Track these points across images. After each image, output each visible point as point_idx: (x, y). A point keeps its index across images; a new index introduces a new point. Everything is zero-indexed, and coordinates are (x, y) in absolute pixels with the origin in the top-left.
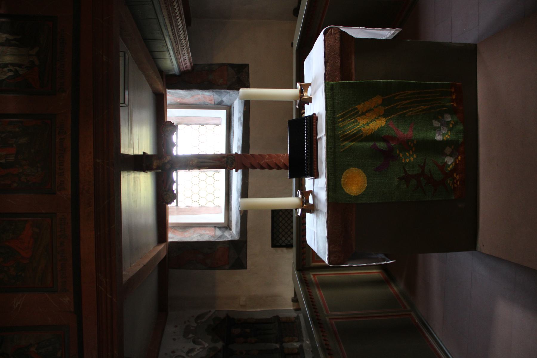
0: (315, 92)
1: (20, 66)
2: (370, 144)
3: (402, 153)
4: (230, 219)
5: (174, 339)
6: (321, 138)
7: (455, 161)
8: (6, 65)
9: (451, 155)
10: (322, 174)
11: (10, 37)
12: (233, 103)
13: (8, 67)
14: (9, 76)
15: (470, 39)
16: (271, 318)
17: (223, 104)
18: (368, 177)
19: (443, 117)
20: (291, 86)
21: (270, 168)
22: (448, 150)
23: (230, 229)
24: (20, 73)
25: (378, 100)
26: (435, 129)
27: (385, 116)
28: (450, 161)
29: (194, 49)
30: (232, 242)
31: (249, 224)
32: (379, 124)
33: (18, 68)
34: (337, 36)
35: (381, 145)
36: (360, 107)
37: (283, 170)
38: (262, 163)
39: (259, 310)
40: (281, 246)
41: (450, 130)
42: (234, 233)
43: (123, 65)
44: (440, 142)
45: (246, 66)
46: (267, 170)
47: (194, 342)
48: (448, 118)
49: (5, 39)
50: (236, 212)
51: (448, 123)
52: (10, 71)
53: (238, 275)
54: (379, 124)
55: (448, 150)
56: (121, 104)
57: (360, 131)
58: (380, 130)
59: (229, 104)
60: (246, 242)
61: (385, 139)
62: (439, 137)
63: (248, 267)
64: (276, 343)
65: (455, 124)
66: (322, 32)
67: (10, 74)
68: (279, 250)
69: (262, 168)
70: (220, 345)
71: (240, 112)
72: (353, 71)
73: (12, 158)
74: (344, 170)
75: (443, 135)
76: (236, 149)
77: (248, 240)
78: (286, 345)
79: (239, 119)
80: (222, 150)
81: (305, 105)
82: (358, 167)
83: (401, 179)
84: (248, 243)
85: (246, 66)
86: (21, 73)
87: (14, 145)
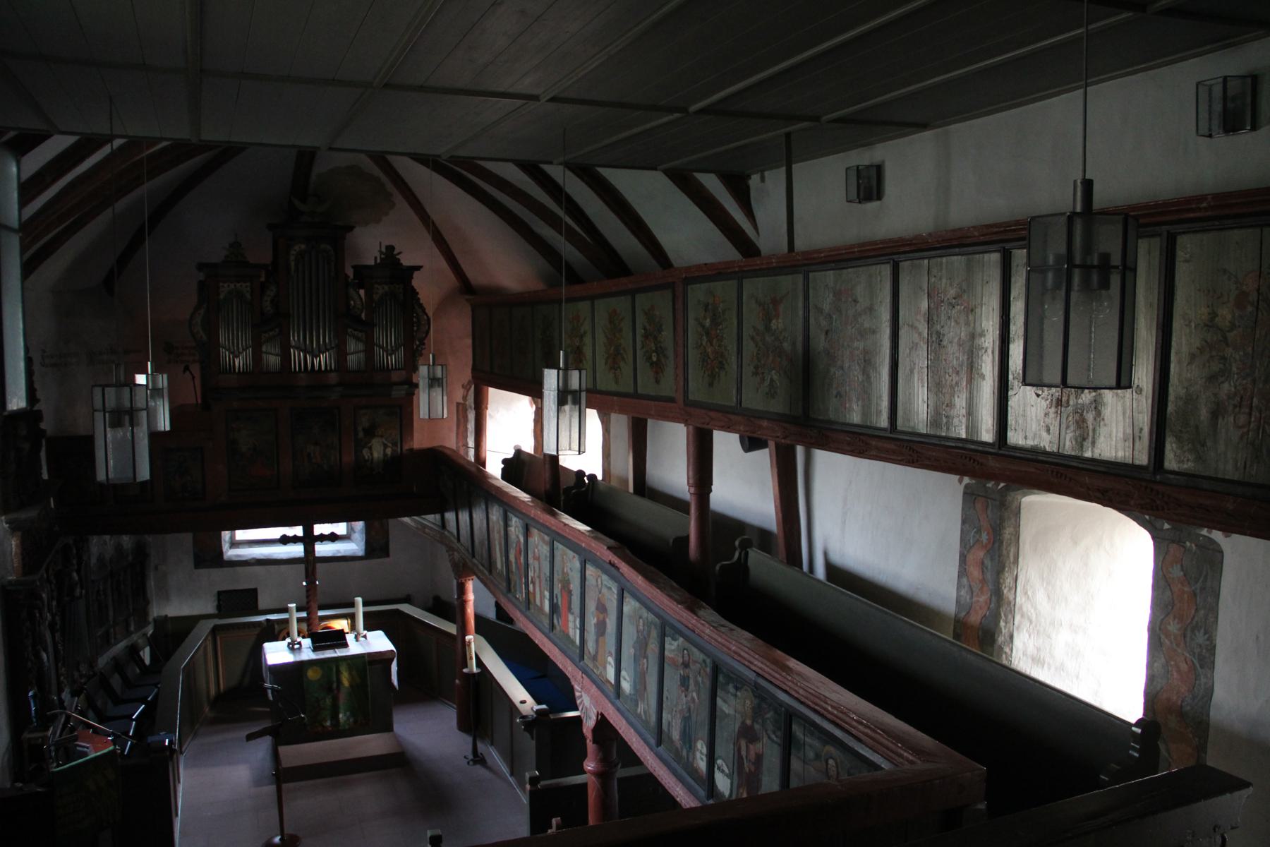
0: (361, 644)
2: (335, 679)
3: (975, 484)
4: (240, 546)
6: (336, 652)
8: (372, 454)
9: (331, 724)
10: (317, 655)
12: (353, 542)
15: (396, 727)
17: (352, 533)
28: (328, 723)
30: (221, 553)
31: (239, 569)
32: (346, 683)
35: (335, 686)
40: (219, 600)
41: (345, 722)
44: (338, 716)
45: (388, 555)
48: (351, 720)
50: (250, 555)
53: (188, 561)
54: (346, 683)
57: (342, 673)
59: (352, 538)
62: (341, 716)
66: (395, 650)
67: (367, 457)
68: (216, 598)
70: (130, 558)
71: (345, 551)
79: (338, 551)
84: (221, 569)
85: (388, 555)
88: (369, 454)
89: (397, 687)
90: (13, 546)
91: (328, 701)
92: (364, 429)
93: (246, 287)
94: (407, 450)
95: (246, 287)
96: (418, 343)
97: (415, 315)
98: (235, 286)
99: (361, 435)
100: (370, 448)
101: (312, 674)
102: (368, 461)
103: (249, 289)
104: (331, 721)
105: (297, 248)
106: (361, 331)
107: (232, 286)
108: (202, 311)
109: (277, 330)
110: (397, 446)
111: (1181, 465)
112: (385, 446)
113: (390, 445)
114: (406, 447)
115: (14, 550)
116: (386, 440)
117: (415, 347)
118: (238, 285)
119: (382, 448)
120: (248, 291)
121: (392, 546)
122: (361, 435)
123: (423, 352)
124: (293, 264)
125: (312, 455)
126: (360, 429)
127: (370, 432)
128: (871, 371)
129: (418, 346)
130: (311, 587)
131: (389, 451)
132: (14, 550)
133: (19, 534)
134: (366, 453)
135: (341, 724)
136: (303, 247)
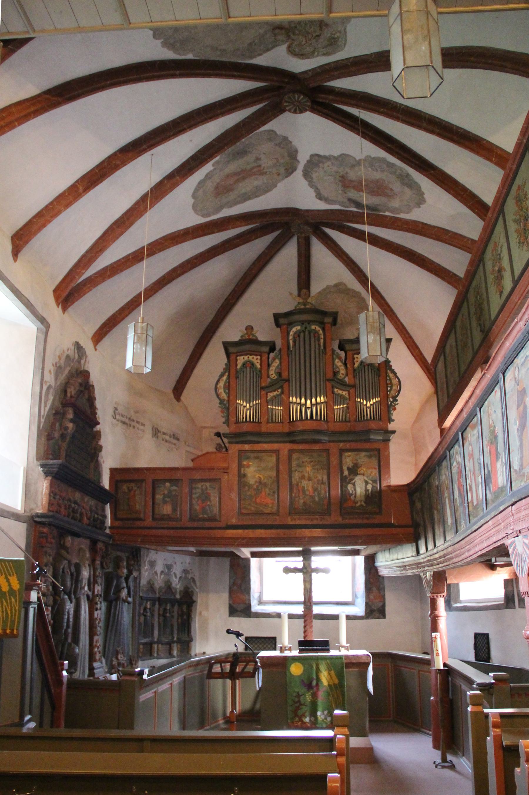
1: (355, 496)
2: (315, 677)
5: (182, 563)
7: (308, 723)
8: (355, 489)
9: (310, 720)
11: (370, 492)
18: (299, 676)
19: (329, 716)
20: (348, 642)
21: (305, 632)
22: (313, 719)
23: (259, 605)
25: (336, 681)
26: (323, 712)
27: (329, 685)
29: (394, 579)
30: (249, 606)
34: (367, 661)
35: (314, 683)
36: (333, 672)
37: (303, 635)
38: (307, 627)
41: (323, 720)
42: (256, 607)
45: (384, 616)
46: (303, 630)
47: (180, 578)
51: (326, 719)
52: (352, 491)
53: (225, 610)
55: (313, 719)
57: (321, 672)
58: (322, 683)
59: (356, 603)
60: (250, 617)
61: (317, 685)
62: (319, 713)
63: (230, 618)
64: (177, 638)
65: (326, 723)
67: (351, 492)
69: (305, 627)
70: (178, 596)
72: (351, 670)
74: (302, 664)
75: (320, 716)
76: (316, 610)
77: (251, 619)
78: (175, 645)
80: (315, 599)
82: (304, 671)
83: (298, 693)
84: (249, 619)
85: (384, 616)
88: (353, 489)
89: (372, 693)
90: (44, 488)
91: (308, 698)
92: (348, 469)
93: (257, 359)
95: (257, 359)
96: (392, 400)
98: (248, 357)
99: (346, 473)
100: (354, 485)
101: (296, 670)
102: (352, 494)
103: (259, 361)
104: (310, 717)
105: (294, 329)
107: (246, 358)
108: (225, 378)
109: (280, 390)
110: (377, 483)
112: (367, 483)
113: (370, 482)
114: (384, 484)
115: (44, 491)
116: (367, 477)
117: (389, 403)
118: (251, 357)
119: (364, 484)
121: (388, 609)
122: (346, 473)
123: (396, 406)
124: (291, 342)
126: (345, 468)
127: (354, 470)
129: (392, 402)
130: (308, 603)
131: (369, 487)
132: (44, 491)
133: (50, 478)
134: (350, 487)
135: (319, 722)
136: (299, 328)
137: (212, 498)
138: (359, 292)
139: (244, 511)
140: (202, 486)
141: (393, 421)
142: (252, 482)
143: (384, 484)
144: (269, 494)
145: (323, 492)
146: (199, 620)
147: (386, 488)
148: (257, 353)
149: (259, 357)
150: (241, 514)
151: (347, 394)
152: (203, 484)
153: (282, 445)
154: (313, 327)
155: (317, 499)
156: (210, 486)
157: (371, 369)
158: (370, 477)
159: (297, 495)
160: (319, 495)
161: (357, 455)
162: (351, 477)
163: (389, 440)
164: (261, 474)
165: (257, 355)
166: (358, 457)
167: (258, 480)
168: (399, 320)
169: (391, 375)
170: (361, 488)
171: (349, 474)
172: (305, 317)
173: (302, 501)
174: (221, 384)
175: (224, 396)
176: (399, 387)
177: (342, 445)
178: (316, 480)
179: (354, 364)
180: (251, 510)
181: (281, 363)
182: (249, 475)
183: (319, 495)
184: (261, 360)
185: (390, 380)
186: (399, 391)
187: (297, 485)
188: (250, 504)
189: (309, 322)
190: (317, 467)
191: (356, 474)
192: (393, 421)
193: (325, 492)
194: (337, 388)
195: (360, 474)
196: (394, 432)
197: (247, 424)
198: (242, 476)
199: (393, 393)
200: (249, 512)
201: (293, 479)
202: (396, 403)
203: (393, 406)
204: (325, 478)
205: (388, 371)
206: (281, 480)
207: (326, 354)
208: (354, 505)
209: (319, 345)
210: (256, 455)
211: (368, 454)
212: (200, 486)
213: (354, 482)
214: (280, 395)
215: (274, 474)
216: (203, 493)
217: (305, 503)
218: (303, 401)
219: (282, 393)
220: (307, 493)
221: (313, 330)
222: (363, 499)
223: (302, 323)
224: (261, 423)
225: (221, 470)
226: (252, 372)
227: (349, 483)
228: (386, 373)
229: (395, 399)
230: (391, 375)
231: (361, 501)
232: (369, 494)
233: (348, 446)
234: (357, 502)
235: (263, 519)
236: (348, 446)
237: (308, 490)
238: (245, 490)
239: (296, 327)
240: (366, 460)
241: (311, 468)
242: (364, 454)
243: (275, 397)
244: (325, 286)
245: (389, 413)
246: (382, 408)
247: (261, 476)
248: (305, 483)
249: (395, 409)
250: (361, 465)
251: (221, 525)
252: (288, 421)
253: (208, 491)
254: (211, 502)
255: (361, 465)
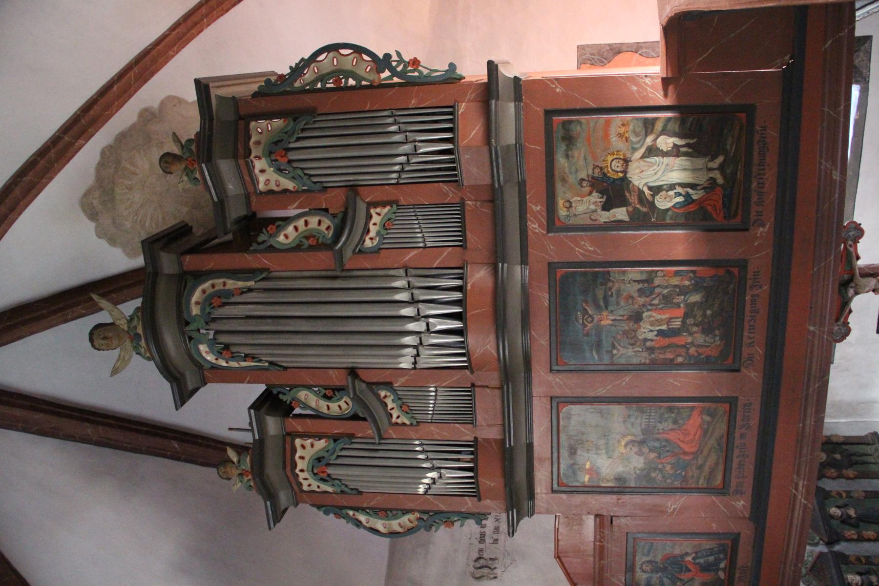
1: (693, 186)
8: (672, 187)
13: (675, 189)
14: (678, 203)
16: (866, 435)
24: (694, 198)
33: (690, 191)
39: (843, 421)
43: (475, 74)
49: (672, 145)
52: (680, 194)
56: (422, 66)
67: (680, 199)
73: (678, 323)
81: (294, 67)
86: (695, 197)
87: (682, 305)
88: (671, 193)
92: (606, 207)
93: (303, 447)
94: (666, 95)
95: (303, 447)
96: (387, 73)
97: (319, 85)
100: (656, 190)
102: (687, 196)
106: (369, 217)
108: (362, 518)
109: (383, 393)
110: (655, 119)
111: (670, 217)
112: (652, 151)
113: (649, 140)
114: (658, 97)
116: (634, 150)
117: (396, 80)
118: (301, 465)
120: (312, 446)
122: (620, 213)
125: (664, 327)
126: (604, 217)
128: (757, 375)
131: (666, 142)
134: (663, 203)
137: (677, 551)
138: (103, 153)
139: (718, 480)
140: (644, 571)
141: (452, 66)
142: (638, 462)
143: (658, 97)
144: (675, 422)
145: (675, 281)
146: (834, 417)
147: (671, 88)
148: (288, 447)
149: (298, 442)
150: (723, 490)
151: (378, 210)
152: (638, 570)
153: (537, 390)
154: (195, 310)
155: (695, 298)
156: (644, 555)
157: (299, 139)
158: (634, 139)
159: (683, 351)
160: (684, 291)
161: (564, 180)
162: (633, 199)
163: (516, 80)
164: (619, 442)
165: (294, 451)
166: (572, 179)
167: (635, 449)
168: (164, 37)
169: (309, 75)
170: (669, 169)
171: (623, 203)
172: (170, 340)
173: (700, 338)
174: (379, 525)
175: (406, 520)
176: (344, 52)
177: (534, 227)
178: (641, 300)
179: (286, 191)
180: (717, 464)
181: (309, 387)
182: (620, 469)
183: (684, 291)
184: (304, 435)
185: (322, 78)
186: (359, 50)
187: (651, 350)
188: (700, 468)
189: (183, 322)
190: (600, 293)
191: (624, 182)
192: (452, 66)
193: (677, 273)
194: (362, 241)
195: (625, 172)
196: (492, 67)
197: (481, 480)
198: (620, 488)
199: (365, 68)
200: (721, 467)
201: (635, 361)
202: (395, 57)
203: (404, 71)
204: (634, 273)
205: (297, 84)
206: (636, 393)
207: (267, 270)
208: (719, 191)
209: (242, 292)
210: (564, 453)
211: (560, 149)
212: (645, 576)
213: (650, 188)
214: (394, 391)
215: (617, 410)
216: (664, 569)
217: (707, 330)
218: (408, 340)
219: (388, 385)
220: (677, 324)
221: (203, 310)
222: (700, 162)
223: (189, 338)
224: (476, 438)
225: (606, 532)
226: (339, 461)
227: (652, 205)
228: (302, 91)
229: (383, 62)
230: (309, 75)
231: (710, 170)
232: (687, 145)
233: (536, 208)
234: (713, 180)
235: (742, 435)
236: (536, 208)
237: (669, 321)
238: (660, 477)
239: (204, 355)
240: (580, 152)
241: (605, 313)
242: (561, 161)
243: (403, 407)
244: (103, 243)
245: (427, 82)
246: (413, 103)
247: (623, 443)
248: (646, 331)
249: (415, 62)
250: (595, 167)
251: (747, 531)
252: (467, 372)
253: (659, 558)
254: (687, 554)
255: (595, 167)
